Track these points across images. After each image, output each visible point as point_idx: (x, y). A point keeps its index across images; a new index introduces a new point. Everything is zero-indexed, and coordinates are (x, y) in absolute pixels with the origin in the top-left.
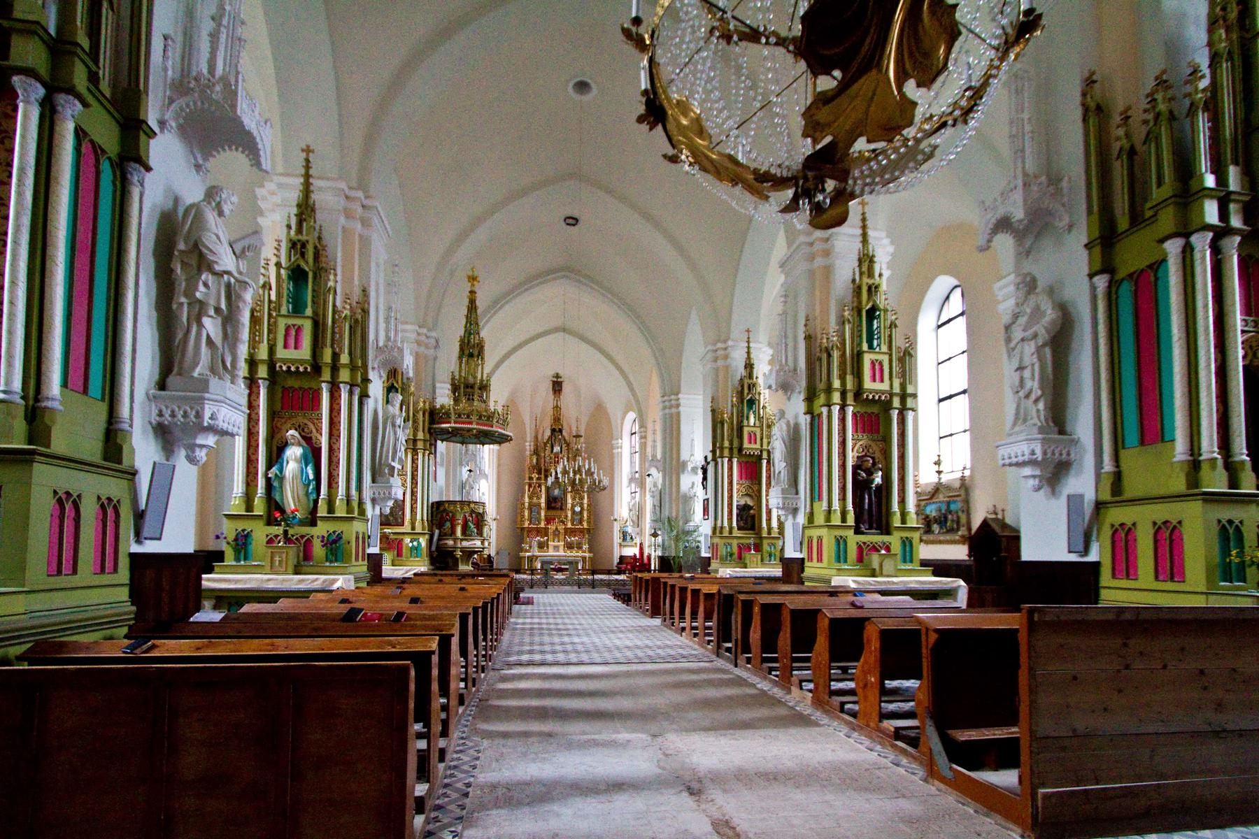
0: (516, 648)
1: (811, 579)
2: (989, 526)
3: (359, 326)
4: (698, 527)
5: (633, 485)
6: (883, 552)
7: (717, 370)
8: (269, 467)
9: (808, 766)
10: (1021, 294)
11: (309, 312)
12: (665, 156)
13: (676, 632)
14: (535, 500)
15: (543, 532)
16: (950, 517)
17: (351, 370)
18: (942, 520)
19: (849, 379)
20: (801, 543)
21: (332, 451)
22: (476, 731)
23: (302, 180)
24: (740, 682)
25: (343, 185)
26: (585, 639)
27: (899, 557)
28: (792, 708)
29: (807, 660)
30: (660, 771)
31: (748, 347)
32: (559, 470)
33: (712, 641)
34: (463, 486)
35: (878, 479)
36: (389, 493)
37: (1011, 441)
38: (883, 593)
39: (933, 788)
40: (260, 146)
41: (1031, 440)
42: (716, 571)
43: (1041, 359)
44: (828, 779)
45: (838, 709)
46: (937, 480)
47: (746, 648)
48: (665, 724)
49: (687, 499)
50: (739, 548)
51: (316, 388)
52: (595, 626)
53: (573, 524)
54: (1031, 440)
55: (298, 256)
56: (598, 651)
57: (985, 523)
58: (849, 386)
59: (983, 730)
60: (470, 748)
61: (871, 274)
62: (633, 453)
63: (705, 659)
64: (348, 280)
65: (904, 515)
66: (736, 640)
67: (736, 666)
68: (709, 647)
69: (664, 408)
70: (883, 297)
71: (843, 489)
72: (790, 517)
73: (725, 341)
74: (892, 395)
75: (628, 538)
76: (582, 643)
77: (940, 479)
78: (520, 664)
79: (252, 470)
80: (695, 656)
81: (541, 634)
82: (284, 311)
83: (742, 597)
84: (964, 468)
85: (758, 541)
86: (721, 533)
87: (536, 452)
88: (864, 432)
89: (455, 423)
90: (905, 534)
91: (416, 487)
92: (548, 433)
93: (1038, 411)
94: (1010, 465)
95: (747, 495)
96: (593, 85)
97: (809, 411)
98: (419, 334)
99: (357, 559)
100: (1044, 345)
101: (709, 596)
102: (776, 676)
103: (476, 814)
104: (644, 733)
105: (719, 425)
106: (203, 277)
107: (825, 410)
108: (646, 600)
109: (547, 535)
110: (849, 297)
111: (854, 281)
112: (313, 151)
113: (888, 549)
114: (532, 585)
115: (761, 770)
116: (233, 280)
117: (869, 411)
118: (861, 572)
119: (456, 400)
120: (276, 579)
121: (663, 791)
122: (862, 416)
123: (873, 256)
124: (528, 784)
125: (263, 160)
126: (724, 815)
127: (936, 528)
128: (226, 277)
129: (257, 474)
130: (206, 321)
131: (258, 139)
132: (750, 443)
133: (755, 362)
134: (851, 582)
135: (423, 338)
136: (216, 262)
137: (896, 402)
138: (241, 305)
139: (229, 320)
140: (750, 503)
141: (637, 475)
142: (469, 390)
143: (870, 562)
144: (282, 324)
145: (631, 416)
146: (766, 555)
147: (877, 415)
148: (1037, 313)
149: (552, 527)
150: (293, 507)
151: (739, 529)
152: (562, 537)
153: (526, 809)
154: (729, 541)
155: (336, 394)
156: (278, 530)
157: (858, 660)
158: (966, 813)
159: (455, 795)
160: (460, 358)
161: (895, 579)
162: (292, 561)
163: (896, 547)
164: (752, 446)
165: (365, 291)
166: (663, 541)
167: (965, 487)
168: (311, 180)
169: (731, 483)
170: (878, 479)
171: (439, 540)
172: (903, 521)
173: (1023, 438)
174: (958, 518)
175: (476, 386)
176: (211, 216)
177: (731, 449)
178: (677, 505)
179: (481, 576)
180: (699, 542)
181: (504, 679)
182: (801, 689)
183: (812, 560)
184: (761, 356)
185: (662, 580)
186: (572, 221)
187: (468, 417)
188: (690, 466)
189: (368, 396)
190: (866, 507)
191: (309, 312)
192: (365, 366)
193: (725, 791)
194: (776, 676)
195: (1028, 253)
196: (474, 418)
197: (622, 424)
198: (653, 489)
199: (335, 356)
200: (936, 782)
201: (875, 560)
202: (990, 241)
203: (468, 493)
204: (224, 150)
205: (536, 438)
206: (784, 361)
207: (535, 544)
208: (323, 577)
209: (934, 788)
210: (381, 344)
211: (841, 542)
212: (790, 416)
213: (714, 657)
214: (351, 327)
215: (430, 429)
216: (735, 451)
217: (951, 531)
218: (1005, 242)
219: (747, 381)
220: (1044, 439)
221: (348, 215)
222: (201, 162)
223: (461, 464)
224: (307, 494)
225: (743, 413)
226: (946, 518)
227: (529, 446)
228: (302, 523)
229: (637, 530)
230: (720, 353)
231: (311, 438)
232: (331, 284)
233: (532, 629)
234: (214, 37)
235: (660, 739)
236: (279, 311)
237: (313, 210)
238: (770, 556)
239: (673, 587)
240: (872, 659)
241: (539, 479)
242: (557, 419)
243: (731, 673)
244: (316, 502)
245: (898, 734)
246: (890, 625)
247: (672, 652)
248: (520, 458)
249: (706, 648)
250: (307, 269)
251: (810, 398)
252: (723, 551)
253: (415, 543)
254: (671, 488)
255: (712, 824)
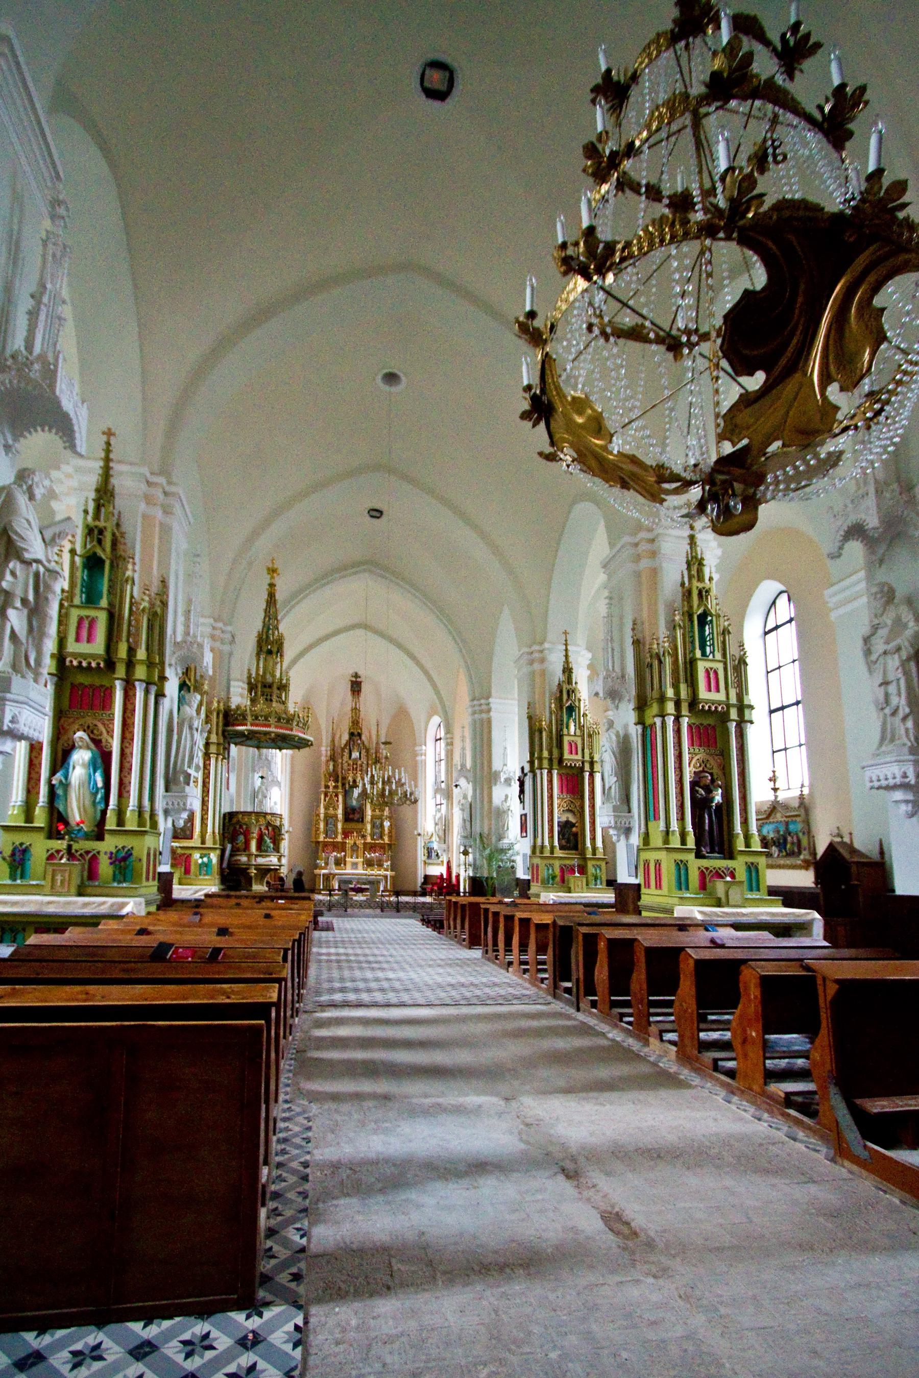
0: (326, 985)
1: (651, 909)
2: (836, 850)
3: (157, 621)
4: (512, 844)
5: (438, 796)
6: (728, 879)
7: (532, 674)
8: (53, 772)
9: (693, 1140)
10: (879, 604)
11: (104, 603)
12: (541, 454)
13: (501, 966)
14: (331, 811)
15: (341, 847)
16: (789, 839)
17: (148, 667)
18: (780, 843)
19: (683, 688)
20: (636, 868)
21: (124, 755)
22: (300, 1092)
23: (101, 464)
24: (585, 1030)
25: (145, 470)
26: (401, 974)
27: (746, 884)
28: (655, 1064)
29: (669, 1004)
30: (522, 1146)
31: (566, 650)
32: (367, 779)
33: (546, 979)
34: (255, 795)
35: (718, 798)
36: (184, 804)
37: (880, 762)
38: (737, 927)
39: (843, 1170)
40: (76, 428)
41: (899, 761)
42: (538, 896)
43: (906, 673)
44: (719, 1157)
45: (711, 1066)
46: (773, 798)
47: (590, 990)
48: (516, 1083)
49: (500, 814)
50: (562, 870)
51: (108, 685)
52: (409, 959)
53: (372, 839)
54: (899, 761)
55: (95, 543)
56: (419, 990)
57: (831, 847)
58: (684, 694)
59: (894, 1098)
60: (298, 1114)
61: (700, 578)
62: (438, 762)
63: (541, 1001)
64: (147, 569)
65: (747, 837)
66: (578, 980)
67: (578, 1010)
68: (543, 986)
69: (474, 713)
70: (714, 602)
71: (681, 807)
72: (623, 837)
73: (541, 643)
74: (729, 706)
75: (434, 854)
76: (399, 980)
77: (776, 797)
78: (334, 1005)
79: (34, 775)
80: (529, 996)
81: (351, 969)
82: (77, 601)
83: (584, 930)
84: (802, 786)
85: (581, 862)
86: (542, 852)
87: (333, 758)
88: (700, 746)
89: (252, 725)
90: (751, 859)
91: (208, 795)
92: (346, 737)
93: (907, 730)
94: (879, 788)
95: (569, 811)
96: (403, 378)
97: (641, 722)
98: (214, 628)
99: (147, 879)
100: (909, 659)
101: (541, 927)
102: (629, 1023)
103: (321, 1205)
104: (492, 1094)
105: (537, 734)
106: (11, 565)
107: (658, 721)
108: (463, 927)
109: (344, 850)
110: (678, 603)
111: (683, 584)
112: (114, 434)
113: (733, 876)
114: (330, 907)
115: (641, 1145)
116: (42, 570)
117: (706, 722)
118: (707, 901)
119: (253, 701)
120: (58, 902)
121: (534, 1173)
122: (698, 727)
123: (702, 559)
124: (375, 1163)
125: (78, 442)
126: (613, 1206)
127: (775, 850)
128: (34, 565)
129: (39, 780)
130: (11, 613)
131: (74, 421)
132: (571, 753)
133: (574, 665)
134: (696, 912)
135: (218, 632)
136: (26, 550)
137: (734, 714)
138: (50, 596)
139: (35, 611)
140: (572, 819)
141: (443, 785)
142: (267, 690)
143: (714, 888)
144: (75, 614)
145: (436, 720)
146: (591, 878)
147: (714, 728)
148: (899, 624)
149: (349, 842)
150: (78, 819)
151: (562, 848)
152: (360, 852)
153: (381, 1198)
154: (551, 862)
155: (131, 693)
156: (61, 845)
157: (736, 1008)
158: (891, 1203)
159: (292, 1179)
160: (258, 655)
161: (744, 910)
162: (76, 881)
163: (742, 874)
164: (574, 757)
165: (164, 582)
166: (475, 859)
167: (804, 806)
168: (111, 464)
169: (551, 797)
170: (718, 798)
171: (231, 855)
172: (748, 845)
173: (894, 759)
174: (799, 841)
175: (275, 686)
176: (21, 499)
177: (550, 760)
178: (490, 820)
179: (281, 898)
180: (513, 861)
181: (321, 1024)
182: (662, 1040)
183: (649, 887)
184: (580, 659)
185: (482, 906)
186: (376, 513)
187: (266, 719)
188: (503, 777)
189: (164, 695)
190: (707, 828)
191: (104, 603)
192: (162, 663)
193: (608, 1174)
194: (629, 1023)
195: (881, 562)
196: (272, 720)
197: (426, 730)
198: (463, 801)
199: (132, 651)
200: (847, 1163)
201: (720, 887)
202: (841, 548)
203: (261, 802)
204: (36, 431)
205: (333, 741)
206: (611, 668)
207: (332, 860)
208: (111, 900)
209: (843, 1170)
210: (179, 639)
211: (682, 867)
212: (618, 727)
213: (550, 998)
214: (149, 620)
215: (224, 731)
216: (555, 763)
217: (791, 854)
218: (856, 548)
219: (565, 687)
220: (914, 761)
221: (149, 500)
222: (10, 442)
223: (254, 771)
224: (94, 803)
225: (562, 721)
226: (785, 840)
227: (325, 751)
228: (87, 837)
229: (444, 846)
230: (536, 655)
231: (100, 741)
232: (129, 573)
233: (338, 961)
234: (33, 315)
235: (514, 1104)
236: (72, 601)
237: (112, 495)
238: (596, 879)
239: (496, 914)
240: (752, 1009)
241: (336, 787)
242: (356, 722)
243: (575, 1019)
244: (104, 813)
245: (789, 1100)
246: (770, 970)
247: (502, 992)
248: (314, 767)
249: (539, 988)
250: (103, 557)
251: (641, 706)
252: (544, 873)
253: (205, 859)
254: (482, 802)
255: (602, 1217)
